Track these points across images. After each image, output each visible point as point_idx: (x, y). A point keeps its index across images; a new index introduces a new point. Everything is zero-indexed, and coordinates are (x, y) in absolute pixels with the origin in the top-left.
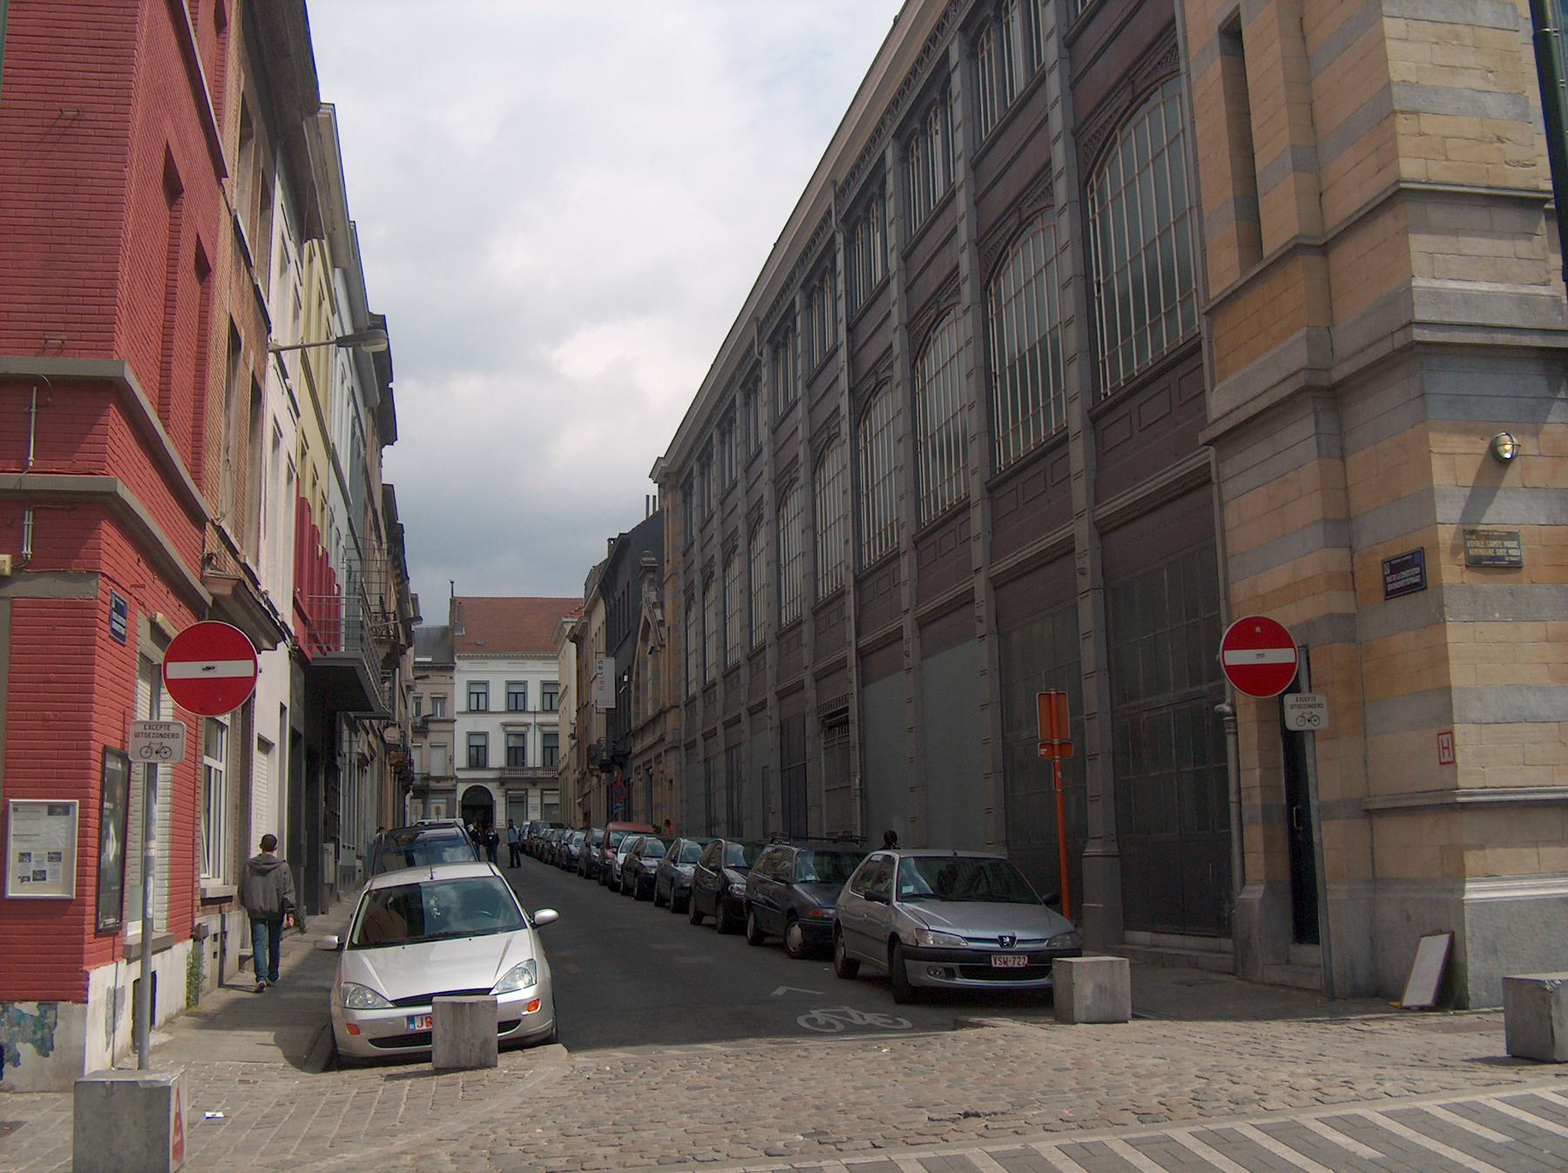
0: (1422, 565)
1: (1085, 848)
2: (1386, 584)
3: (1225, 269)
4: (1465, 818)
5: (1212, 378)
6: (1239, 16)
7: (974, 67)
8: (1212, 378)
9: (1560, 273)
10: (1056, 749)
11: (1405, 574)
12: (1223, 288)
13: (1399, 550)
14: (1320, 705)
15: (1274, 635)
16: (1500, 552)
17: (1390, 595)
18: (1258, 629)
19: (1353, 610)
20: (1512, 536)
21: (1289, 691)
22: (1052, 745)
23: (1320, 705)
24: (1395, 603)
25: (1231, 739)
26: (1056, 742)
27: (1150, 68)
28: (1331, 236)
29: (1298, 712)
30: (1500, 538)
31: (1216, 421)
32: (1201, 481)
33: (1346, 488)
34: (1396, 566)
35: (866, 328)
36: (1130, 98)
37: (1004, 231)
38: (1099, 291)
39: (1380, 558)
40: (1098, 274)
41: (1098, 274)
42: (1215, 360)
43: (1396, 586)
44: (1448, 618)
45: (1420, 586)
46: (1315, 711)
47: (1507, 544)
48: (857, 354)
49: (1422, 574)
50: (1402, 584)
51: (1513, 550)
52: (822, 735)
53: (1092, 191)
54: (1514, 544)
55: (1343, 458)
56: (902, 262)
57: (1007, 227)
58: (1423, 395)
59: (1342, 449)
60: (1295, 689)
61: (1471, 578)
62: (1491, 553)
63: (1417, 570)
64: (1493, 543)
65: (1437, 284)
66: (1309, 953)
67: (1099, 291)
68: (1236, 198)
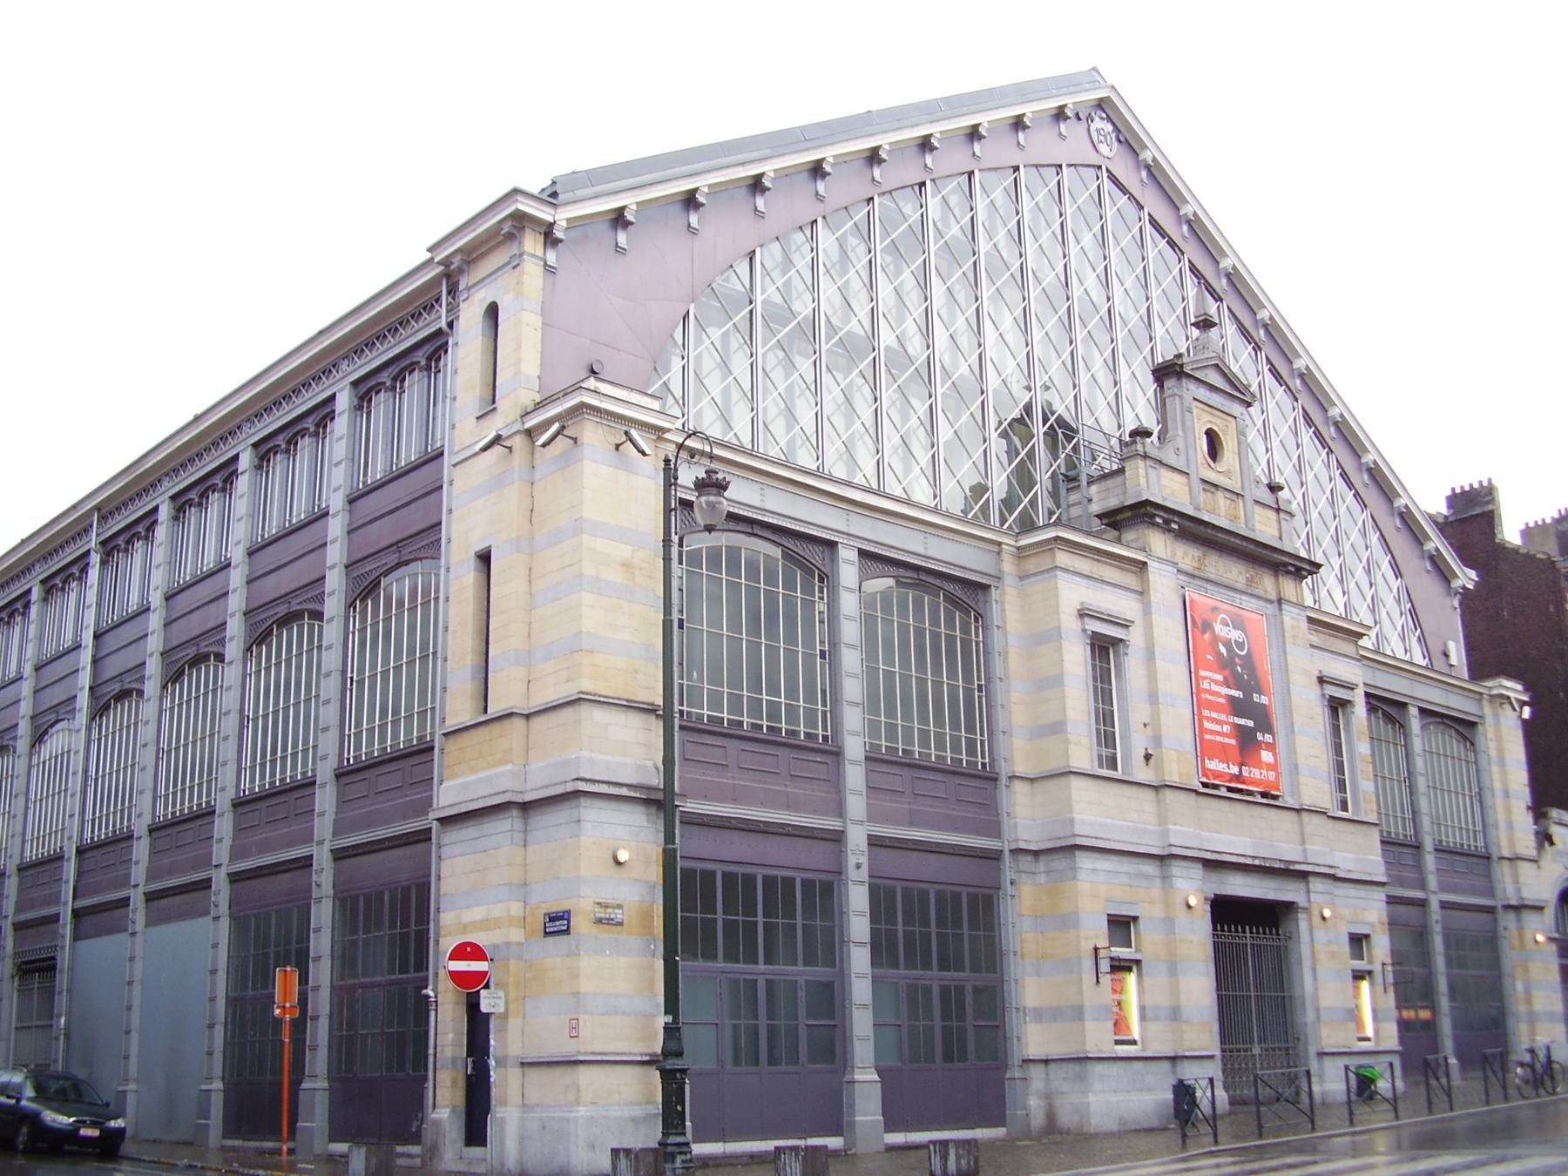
0: (568, 920)
1: (301, 1083)
2: (545, 927)
3: (459, 710)
4: (581, 1068)
5: (441, 774)
6: (490, 551)
7: (259, 477)
8: (441, 774)
9: (908, 1134)
10: (288, 1010)
11: (558, 923)
12: (456, 722)
13: (556, 908)
14: (500, 998)
15: (475, 952)
16: (613, 916)
17: (547, 934)
18: (469, 949)
19: (523, 940)
20: (619, 906)
21: (483, 988)
22: (284, 1007)
23: (500, 998)
24: (551, 939)
25: (432, 1014)
26: (288, 1005)
27: (415, 548)
28: (532, 711)
29: (487, 1001)
30: (613, 907)
31: (444, 807)
32: (424, 836)
33: (526, 865)
34: (553, 918)
35: (112, 641)
36: (396, 561)
37: (272, 613)
38: (352, 684)
39: (543, 911)
40: (352, 672)
41: (352, 672)
42: (323, 672)
43: (552, 930)
44: (582, 953)
45: (567, 931)
46: (498, 1001)
47: (616, 911)
48: (99, 660)
49: (568, 925)
50: (556, 929)
51: (618, 915)
52: (17, 978)
53: (355, 611)
54: (620, 911)
55: (525, 846)
56: (163, 600)
57: (276, 611)
58: (579, 821)
59: (525, 840)
60: (487, 986)
61: (594, 929)
62: (607, 916)
63: (566, 922)
64: (609, 910)
65: (593, 755)
66: (476, 1151)
67: (352, 684)
68: (472, 666)
